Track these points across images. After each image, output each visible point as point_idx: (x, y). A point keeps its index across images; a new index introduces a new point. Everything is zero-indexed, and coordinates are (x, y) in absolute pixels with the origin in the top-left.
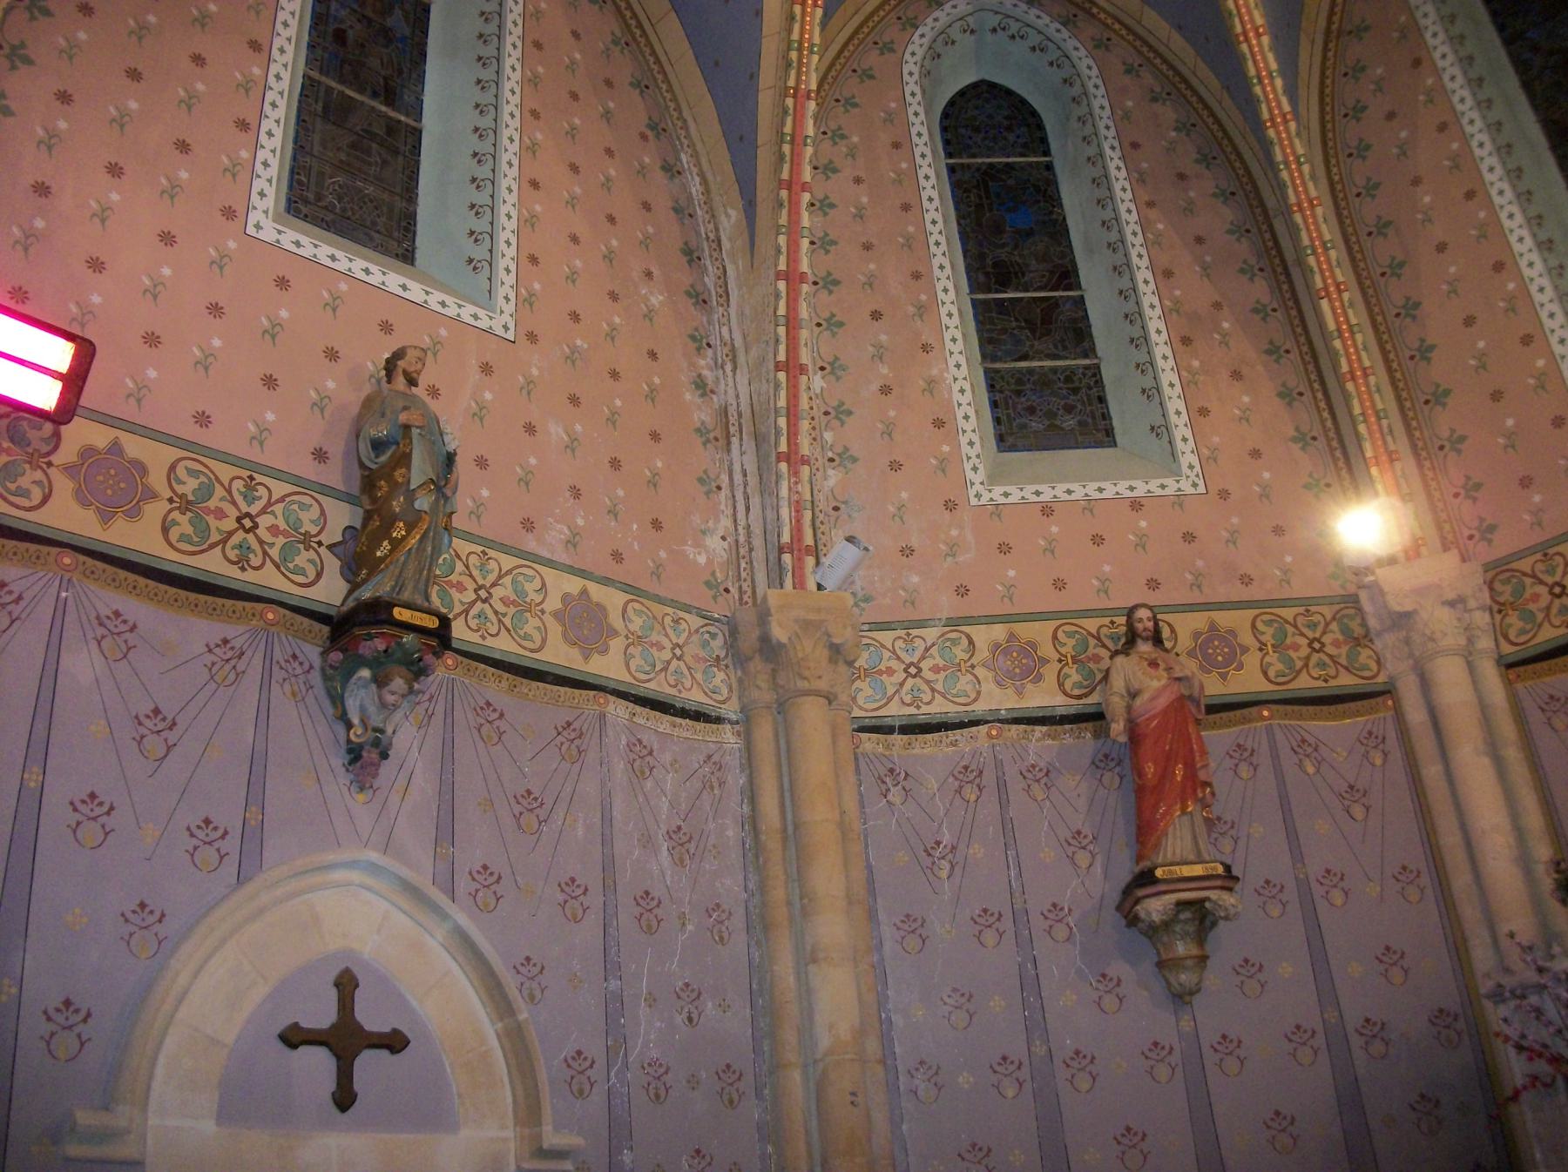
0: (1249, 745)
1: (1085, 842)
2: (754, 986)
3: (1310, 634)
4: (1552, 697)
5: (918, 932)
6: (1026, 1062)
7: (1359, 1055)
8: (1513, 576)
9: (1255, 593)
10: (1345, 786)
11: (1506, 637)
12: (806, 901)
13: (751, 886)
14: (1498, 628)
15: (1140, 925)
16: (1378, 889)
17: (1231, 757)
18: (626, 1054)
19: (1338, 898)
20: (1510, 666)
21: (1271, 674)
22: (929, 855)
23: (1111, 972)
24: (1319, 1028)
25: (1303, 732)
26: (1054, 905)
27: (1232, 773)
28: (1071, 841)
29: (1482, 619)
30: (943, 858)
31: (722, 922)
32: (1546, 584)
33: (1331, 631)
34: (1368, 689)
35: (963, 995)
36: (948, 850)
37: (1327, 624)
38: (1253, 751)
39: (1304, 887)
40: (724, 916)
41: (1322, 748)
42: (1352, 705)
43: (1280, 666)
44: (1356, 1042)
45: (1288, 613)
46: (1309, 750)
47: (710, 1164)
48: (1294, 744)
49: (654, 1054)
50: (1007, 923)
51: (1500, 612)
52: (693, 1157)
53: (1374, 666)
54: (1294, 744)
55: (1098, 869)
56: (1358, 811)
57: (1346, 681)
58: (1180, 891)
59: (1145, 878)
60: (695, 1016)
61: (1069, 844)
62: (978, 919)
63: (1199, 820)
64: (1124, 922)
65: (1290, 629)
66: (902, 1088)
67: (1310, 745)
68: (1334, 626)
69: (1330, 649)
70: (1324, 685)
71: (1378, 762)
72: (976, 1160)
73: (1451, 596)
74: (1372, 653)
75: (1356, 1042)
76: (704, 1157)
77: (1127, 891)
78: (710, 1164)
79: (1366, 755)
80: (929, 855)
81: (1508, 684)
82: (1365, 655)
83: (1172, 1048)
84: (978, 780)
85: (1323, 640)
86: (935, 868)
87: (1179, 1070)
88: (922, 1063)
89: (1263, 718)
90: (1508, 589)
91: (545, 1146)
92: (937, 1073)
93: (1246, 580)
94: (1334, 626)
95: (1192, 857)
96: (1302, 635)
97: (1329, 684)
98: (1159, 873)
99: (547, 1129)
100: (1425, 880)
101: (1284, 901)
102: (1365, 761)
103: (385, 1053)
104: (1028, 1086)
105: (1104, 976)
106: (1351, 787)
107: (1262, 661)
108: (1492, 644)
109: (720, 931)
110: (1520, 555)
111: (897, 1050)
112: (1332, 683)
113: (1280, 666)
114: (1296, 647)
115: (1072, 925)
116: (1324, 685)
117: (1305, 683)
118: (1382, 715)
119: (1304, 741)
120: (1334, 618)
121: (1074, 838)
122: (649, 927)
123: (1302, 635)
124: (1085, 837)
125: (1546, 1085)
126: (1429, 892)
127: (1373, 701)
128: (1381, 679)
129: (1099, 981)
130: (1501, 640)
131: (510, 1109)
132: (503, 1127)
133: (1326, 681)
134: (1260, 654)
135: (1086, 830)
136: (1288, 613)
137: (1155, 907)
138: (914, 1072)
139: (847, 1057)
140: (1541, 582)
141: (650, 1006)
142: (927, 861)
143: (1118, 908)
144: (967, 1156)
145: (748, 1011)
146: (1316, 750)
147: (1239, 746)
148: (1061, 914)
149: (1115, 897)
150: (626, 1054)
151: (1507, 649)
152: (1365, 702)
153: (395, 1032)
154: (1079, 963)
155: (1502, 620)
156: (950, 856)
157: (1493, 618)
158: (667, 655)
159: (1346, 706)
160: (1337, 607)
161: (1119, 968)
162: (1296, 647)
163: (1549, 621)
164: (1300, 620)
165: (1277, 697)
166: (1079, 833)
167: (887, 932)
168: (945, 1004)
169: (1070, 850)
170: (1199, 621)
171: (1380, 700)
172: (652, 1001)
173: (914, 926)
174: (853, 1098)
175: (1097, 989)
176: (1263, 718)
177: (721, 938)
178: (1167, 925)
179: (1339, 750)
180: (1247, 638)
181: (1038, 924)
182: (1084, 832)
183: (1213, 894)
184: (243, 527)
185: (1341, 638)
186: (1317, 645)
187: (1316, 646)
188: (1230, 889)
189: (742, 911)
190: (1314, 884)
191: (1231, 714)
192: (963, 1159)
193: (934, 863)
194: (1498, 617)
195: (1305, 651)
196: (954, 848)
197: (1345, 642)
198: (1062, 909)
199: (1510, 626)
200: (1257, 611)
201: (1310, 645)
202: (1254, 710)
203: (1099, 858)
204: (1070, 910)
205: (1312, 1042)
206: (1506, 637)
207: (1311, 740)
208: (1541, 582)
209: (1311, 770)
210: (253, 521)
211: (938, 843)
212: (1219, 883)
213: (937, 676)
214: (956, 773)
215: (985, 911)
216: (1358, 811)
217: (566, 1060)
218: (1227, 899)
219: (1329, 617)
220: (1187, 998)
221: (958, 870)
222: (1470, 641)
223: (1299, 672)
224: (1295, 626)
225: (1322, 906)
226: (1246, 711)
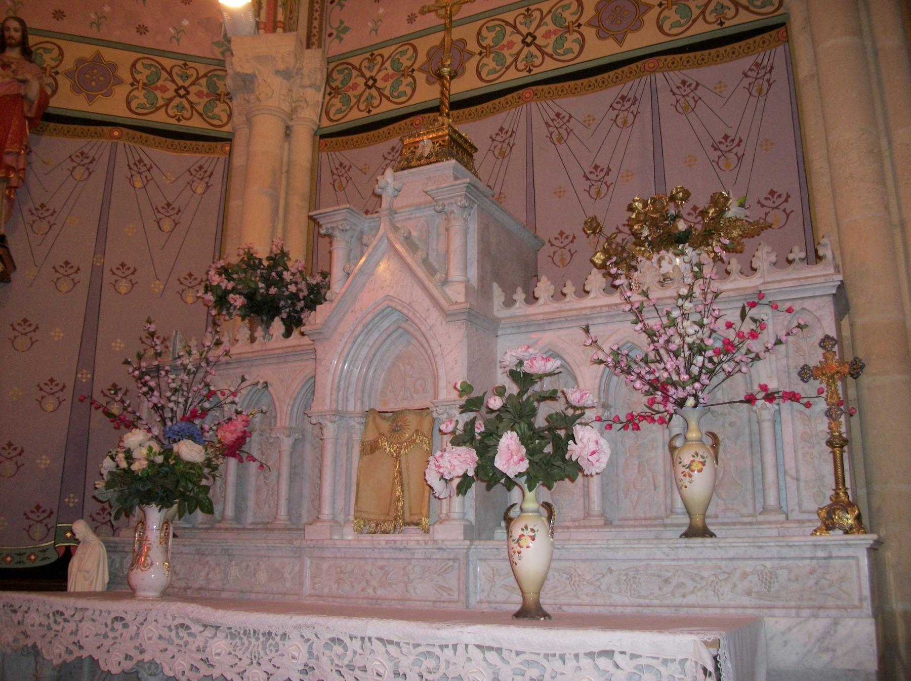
0: (91, 155)
3: (180, 83)
4: (341, 164)
8: (346, 68)
9: (146, 41)
10: (163, 204)
11: (327, 114)
14: (324, 108)
16: (162, 287)
17: (72, 160)
19: (124, 286)
20: (323, 137)
21: (134, 105)
24: (70, 385)
25: (142, 154)
27: (69, 173)
29: (315, 96)
32: (521, 34)
33: (200, 85)
34: (213, 134)
37: (198, 78)
38: (94, 159)
39: (97, 272)
42: (79, 128)
43: (143, 100)
45: (167, 63)
46: (143, 169)
48: (132, 162)
51: (330, 94)
53: (225, 119)
54: (132, 162)
56: (167, 225)
57: (196, 124)
65: (164, 75)
67: (145, 165)
68: (203, 81)
69: (192, 98)
70: (176, 122)
71: (200, 190)
73: (281, 67)
74: (227, 108)
81: (317, 150)
82: (220, 109)
84: (207, 180)
85: (189, 89)
89: (113, 137)
90: (341, 77)
93: (142, 30)
94: (203, 81)
96: (173, 81)
97: (181, 123)
101: (134, 281)
106: (168, 205)
107: (130, 93)
108: (316, 119)
110: (354, 53)
112: (183, 122)
113: (143, 100)
114: (164, 89)
116: (176, 122)
117: (160, 118)
118: (217, 156)
119: (141, 161)
120: (205, 75)
121: (135, 164)
122: (562, 260)
123: (173, 81)
127: (213, 144)
128: (226, 129)
130: (324, 114)
133: (179, 120)
134: (130, 88)
136: (167, 63)
140: (519, 32)
147: (82, 153)
151: (325, 123)
152: (206, 144)
155: (330, 100)
157: (324, 98)
158: (171, 93)
159: (72, 127)
160: (213, 68)
162: (164, 89)
163: (358, 107)
164: (176, 70)
165: (129, 123)
170: (87, 51)
171: (219, 144)
176: (113, 137)
179: (169, 174)
180: (124, 73)
184: (373, 84)
185: (205, 91)
186: (182, 92)
187: (182, 92)
191: (86, 128)
194: (327, 98)
195: (171, 93)
197: (208, 95)
199: (333, 105)
200: (141, 55)
201: (176, 91)
202: (106, 129)
205: (60, 394)
206: (327, 114)
207: (147, 161)
208: (519, 32)
209: (138, 184)
210: (369, 79)
213: (201, 100)
214: (192, 171)
216: (167, 225)
219: (201, 74)
222: (294, 111)
223: (158, 109)
224: (170, 74)
225: (107, 288)
226: (99, 128)
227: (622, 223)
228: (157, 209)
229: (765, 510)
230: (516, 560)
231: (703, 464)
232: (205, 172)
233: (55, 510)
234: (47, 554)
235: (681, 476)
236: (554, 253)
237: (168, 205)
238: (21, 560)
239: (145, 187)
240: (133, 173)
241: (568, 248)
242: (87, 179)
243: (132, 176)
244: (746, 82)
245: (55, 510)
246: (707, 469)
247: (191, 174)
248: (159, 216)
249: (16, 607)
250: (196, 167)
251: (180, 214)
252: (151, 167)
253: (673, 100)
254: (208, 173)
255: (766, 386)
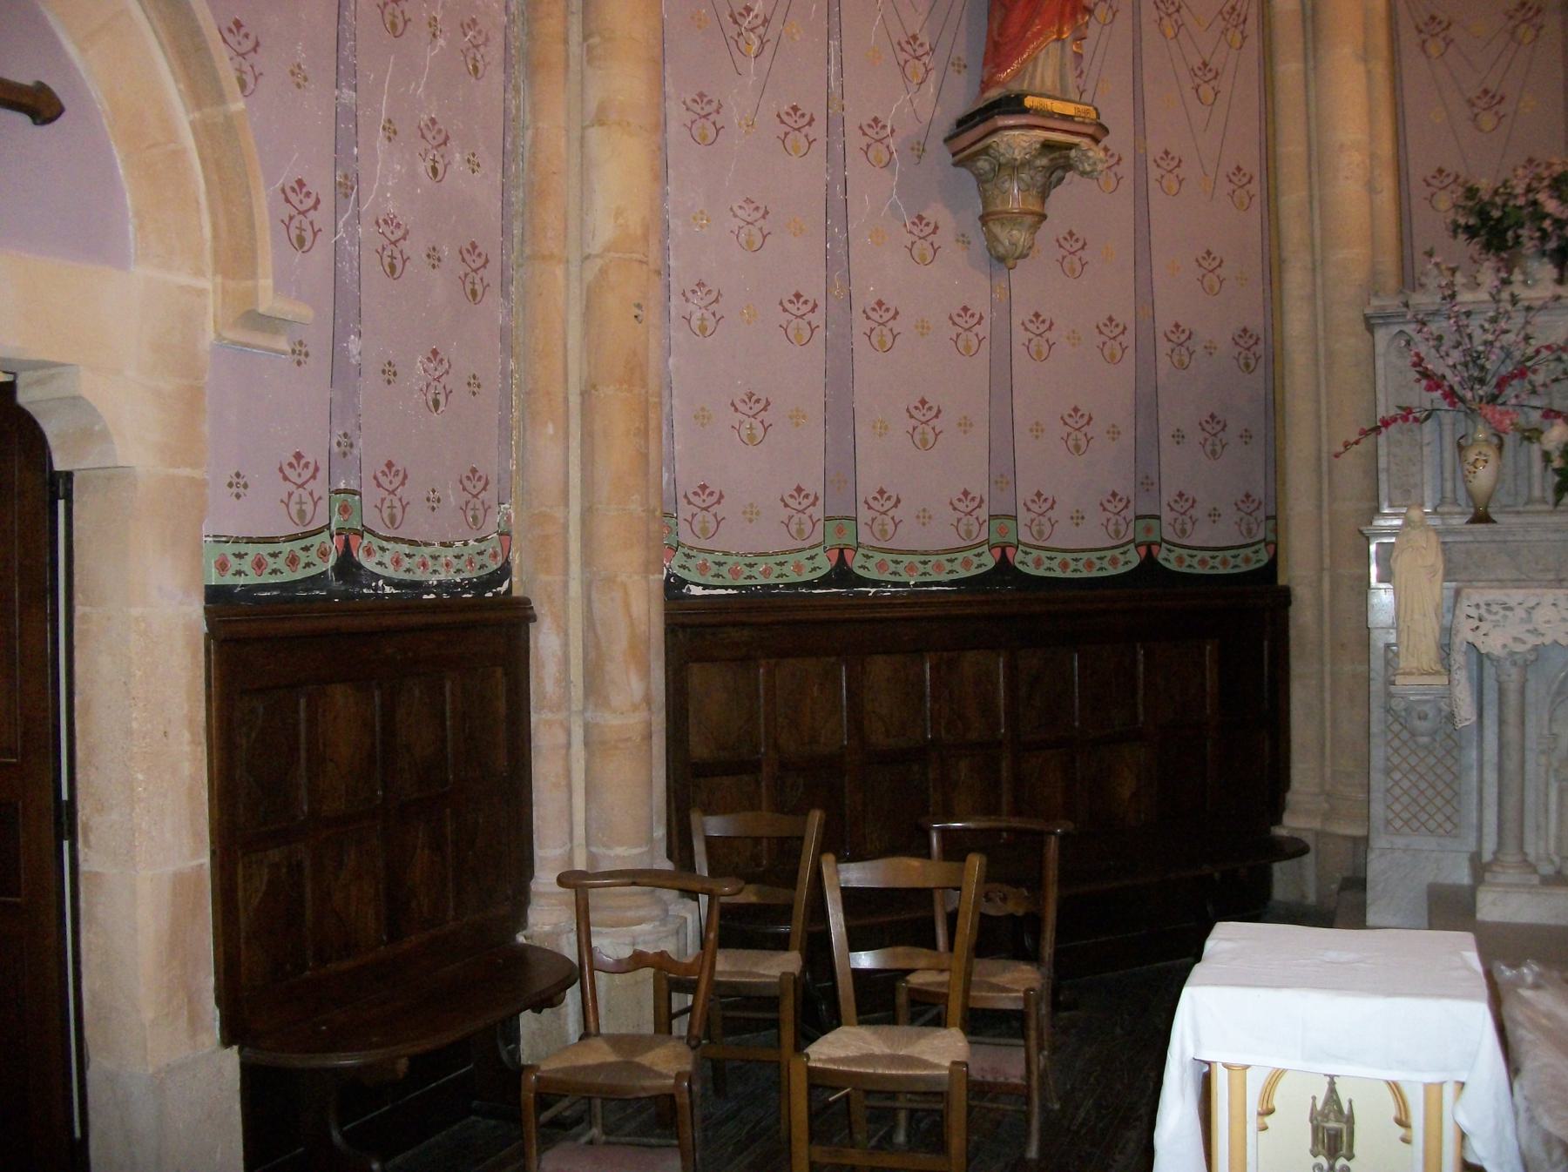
1: (920, 52)
2: (508, 145)
5: (712, 118)
6: (822, 304)
7: (1164, 364)
12: (595, 40)
13: (513, 9)
15: (983, 164)
18: (358, 200)
22: (736, 22)
23: (929, 214)
26: (876, 120)
28: (904, 45)
30: (752, 30)
31: (476, 47)
35: (757, 208)
36: (759, 21)
40: (480, 40)
41: (1184, 11)
44: (1164, 347)
47: (447, 372)
49: (391, 208)
50: (818, 130)
52: (429, 359)
55: (931, 88)
56: (1206, 90)
58: (1054, 130)
59: (1013, 104)
60: (440, 167)
61: (902, 49)
62: (785, 118)
63: (1069, 53)
64: (950, 159)
66: (673, 314)
72: (751, 413)
75: (1164, 347)
76: (441, 361)
77: (965, 123)
78: (447, 372)
79: (1224, 32)
80: (736, 22)
83: (981, 318)
86: (741, 41)
87: (986, 343)
88: (701, 284)
91: (261, 310)
92: (716, 301)
95: (1058, 94)
98: (1029, 102)
99: (266, 283)
100: (1255, 188)
102: (1223, 37)
103: (23, 119)
104: (820, 334)
105: (920, 218)
109: (475, 59)
111: (672, 263)
115: (893, 148)
121: (908, 43)
124: (921, 45)
125: (1416, 420)
126: (1257, 200)
129: (914, 223)
131: (209, 244)
132: (199, 272)
135: (924, 38)
137: (1017, 141)
138: (689, 295)
139: (635, 256)
141: (389, 139)
142: (732, 31)
143: (948, 140)
144: (741, 406)
145: (499, 176)
146: (1178, 11)
148: (883, 134)
149: (946, 125)
150: (358, 200)
153: (42, 89)
154: (895, 196)
156: (761, 30)
161: (936, 212)
166: (915, 38)
167: (675, 111)
168: (735, 216)
169: (902, 56)
172: (391, 132)
173: (708, 109)
174: (637, 312)
175: (911, 232)
177: (476, 68)
178: (1015, 168)
181: (855, 141)
182: (921, 39)
183: (1084, 142)
188: (1097, 141)
189: (500, 38)
190: (1151, 165)
192: (736, 410)
193: (740, 34)
196: (766, 21)
198: (884, 127)
203: (933, 76)
204: (893, 131)
211: (749, 10)
212: (1090, 130)
215: (795, 109)
216: (1206, 90)
217: (283, 191)
218: (1096, 153)
220: (1010, 263)
221: (769, 49)
227: (866, 521)
228: (1193, 69)
229: (1529, 501)
230: (1471, 477)
231: (1486, 461)
232: (1239, 15)
233: (1132, 498)
234: (817, 562)
235: (1467, 473)
236: (873, 520)
237: (1205, 64)
238: (982, 562)
239: (1176, 36)
240: (1163, 15)
241: (891, 513)
242: (1111, 22)
243: (1161, 19)
244: (1512, 23)
245: (1132, 498)
246: (1491, 467)
247: (1224, 19)
248: (1198, 81)
249: (1512, 603)
250: (1228, 8)
251: (1219, 77)
252: (1180, 7)
253: (688, 117)
254: (1242, 18)
255: (1363, 429)
